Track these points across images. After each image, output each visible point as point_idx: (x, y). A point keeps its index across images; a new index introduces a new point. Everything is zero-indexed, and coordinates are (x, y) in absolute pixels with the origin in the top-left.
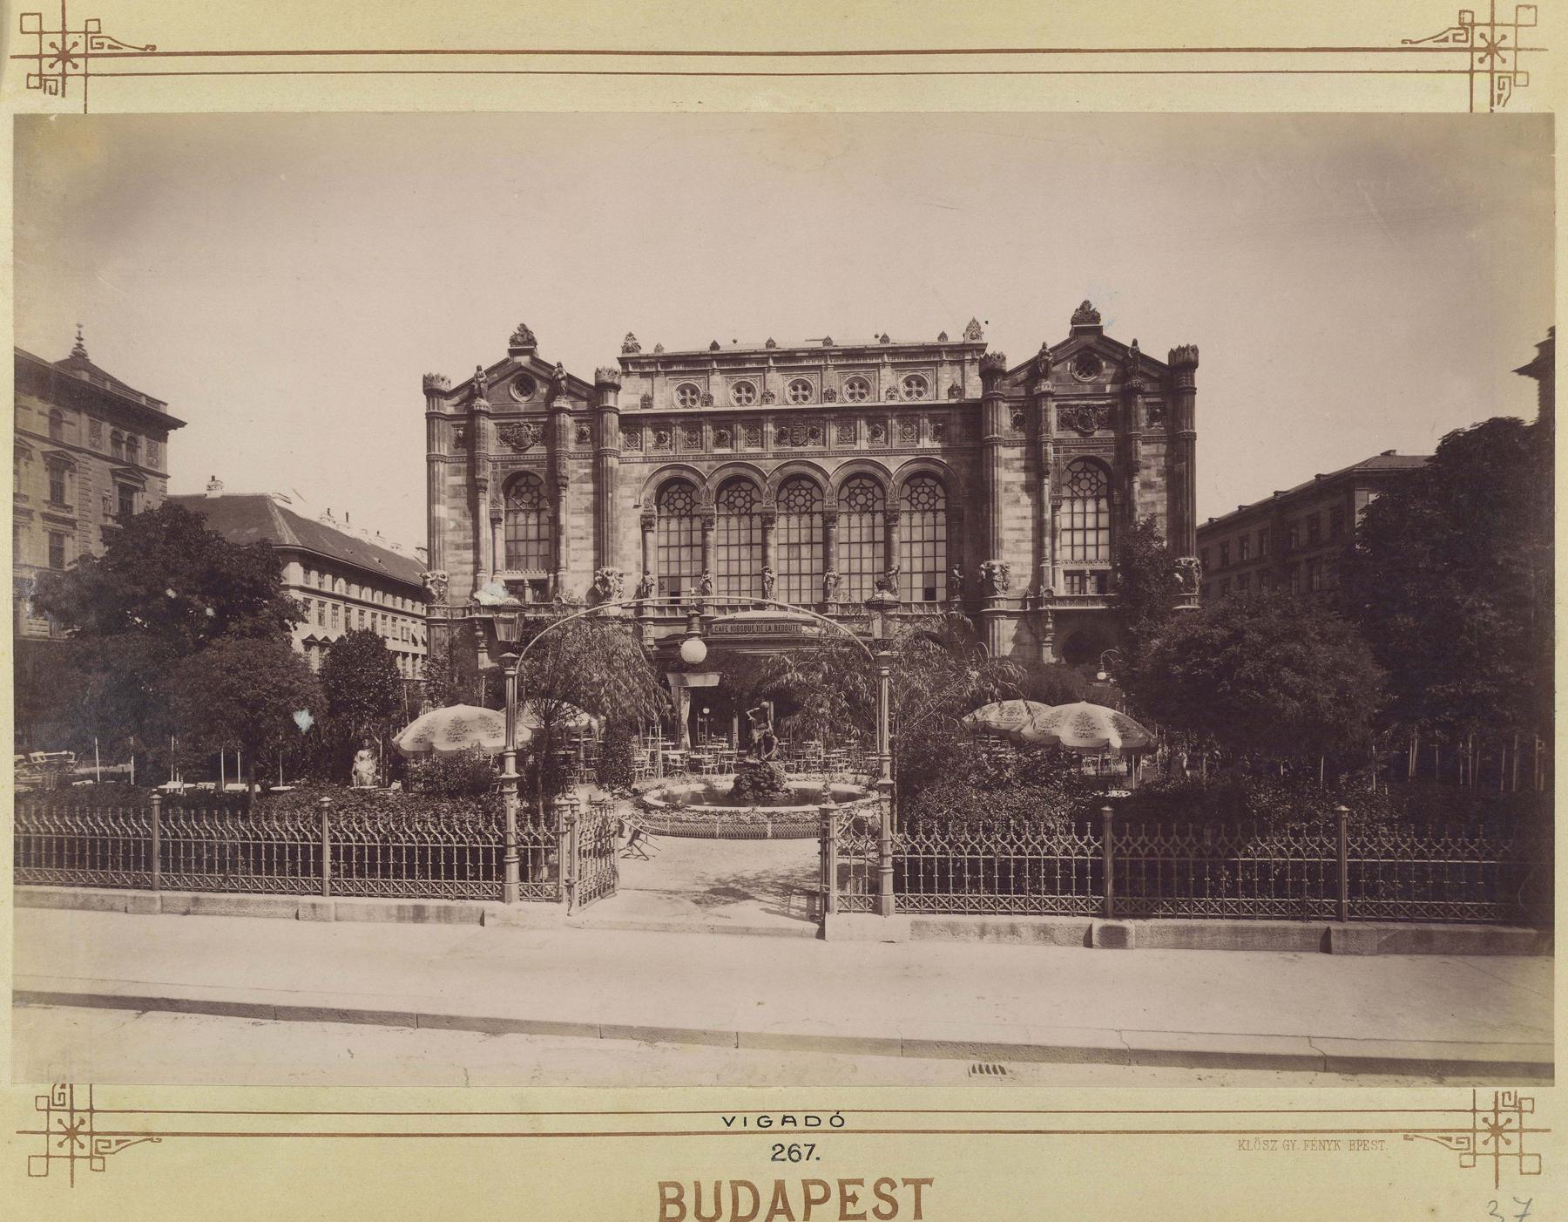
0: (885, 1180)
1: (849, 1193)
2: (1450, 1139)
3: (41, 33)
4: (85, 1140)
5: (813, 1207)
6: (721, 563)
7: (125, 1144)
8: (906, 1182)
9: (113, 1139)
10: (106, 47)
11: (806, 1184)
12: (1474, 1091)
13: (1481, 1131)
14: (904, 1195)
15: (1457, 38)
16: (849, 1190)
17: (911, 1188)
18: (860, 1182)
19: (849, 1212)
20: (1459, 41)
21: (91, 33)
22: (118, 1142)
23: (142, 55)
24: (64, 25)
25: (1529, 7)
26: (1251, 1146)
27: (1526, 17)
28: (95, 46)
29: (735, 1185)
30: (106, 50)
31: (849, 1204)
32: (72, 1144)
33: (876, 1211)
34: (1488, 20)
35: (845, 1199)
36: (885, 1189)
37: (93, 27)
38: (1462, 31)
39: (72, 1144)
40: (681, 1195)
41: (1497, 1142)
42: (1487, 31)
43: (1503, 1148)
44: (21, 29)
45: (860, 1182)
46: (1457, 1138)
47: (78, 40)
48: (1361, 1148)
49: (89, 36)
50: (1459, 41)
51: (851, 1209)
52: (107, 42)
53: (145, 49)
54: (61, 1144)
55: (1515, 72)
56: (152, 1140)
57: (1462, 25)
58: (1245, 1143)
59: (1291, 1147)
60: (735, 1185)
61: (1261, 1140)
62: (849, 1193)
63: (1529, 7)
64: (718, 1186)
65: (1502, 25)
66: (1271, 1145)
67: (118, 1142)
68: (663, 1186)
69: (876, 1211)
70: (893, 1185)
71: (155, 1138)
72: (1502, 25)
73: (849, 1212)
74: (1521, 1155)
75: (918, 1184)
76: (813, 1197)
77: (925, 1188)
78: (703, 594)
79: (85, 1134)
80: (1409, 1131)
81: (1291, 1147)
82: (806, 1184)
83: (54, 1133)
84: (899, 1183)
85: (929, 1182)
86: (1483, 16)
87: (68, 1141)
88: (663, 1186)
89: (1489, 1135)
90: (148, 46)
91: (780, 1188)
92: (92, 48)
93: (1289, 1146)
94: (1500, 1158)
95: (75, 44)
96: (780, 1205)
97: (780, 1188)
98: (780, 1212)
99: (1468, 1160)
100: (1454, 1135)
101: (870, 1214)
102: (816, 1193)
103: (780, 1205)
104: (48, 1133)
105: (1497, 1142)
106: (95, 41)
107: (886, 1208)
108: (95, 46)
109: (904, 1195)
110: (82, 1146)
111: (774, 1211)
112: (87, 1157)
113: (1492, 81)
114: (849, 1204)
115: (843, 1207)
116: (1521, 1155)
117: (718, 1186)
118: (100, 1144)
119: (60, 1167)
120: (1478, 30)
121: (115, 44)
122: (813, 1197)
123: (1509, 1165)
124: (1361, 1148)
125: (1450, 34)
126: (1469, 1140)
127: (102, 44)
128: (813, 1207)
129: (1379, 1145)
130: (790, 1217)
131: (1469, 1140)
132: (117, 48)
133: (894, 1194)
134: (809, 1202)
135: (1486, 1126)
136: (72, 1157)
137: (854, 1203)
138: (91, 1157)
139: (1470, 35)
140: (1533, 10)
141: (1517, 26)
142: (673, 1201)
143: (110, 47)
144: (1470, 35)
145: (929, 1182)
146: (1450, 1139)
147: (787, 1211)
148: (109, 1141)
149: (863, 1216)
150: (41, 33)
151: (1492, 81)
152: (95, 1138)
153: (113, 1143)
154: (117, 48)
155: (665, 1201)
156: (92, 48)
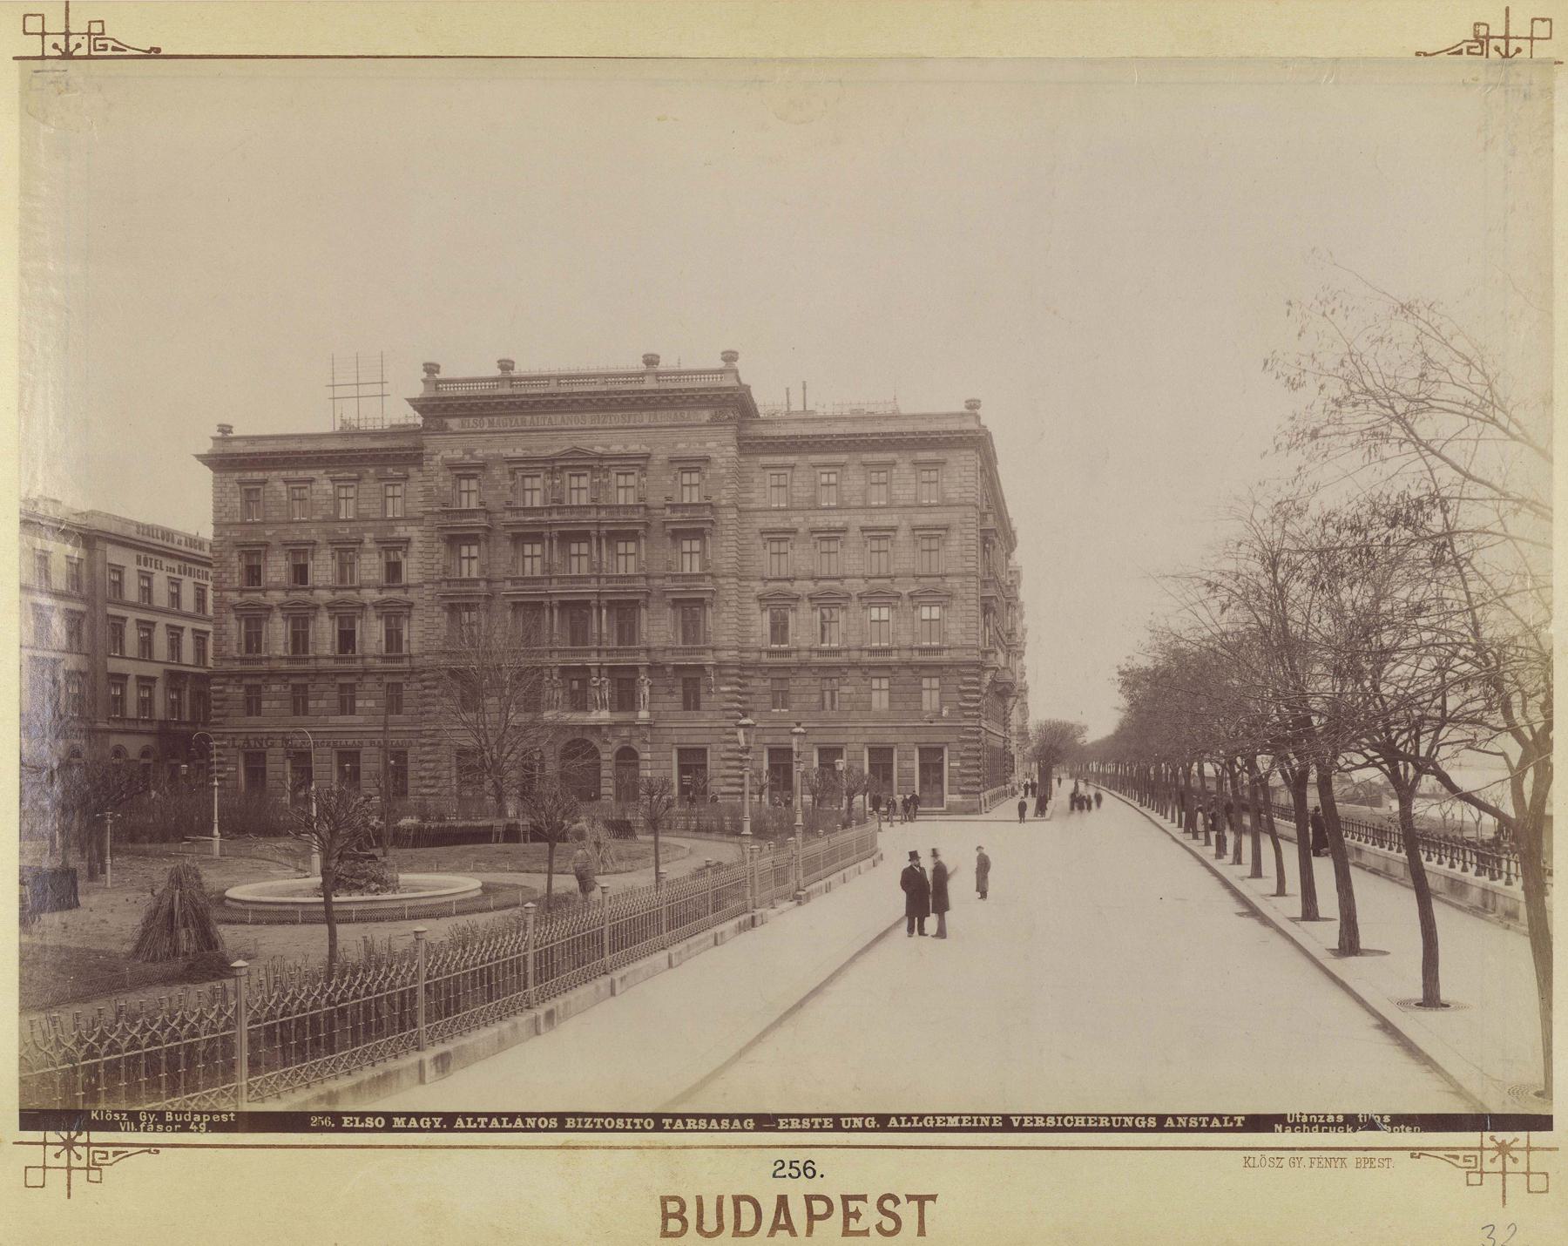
0: (891, 1197)
1: (852, 1209)
2: (1457, 1157)
3: (43, 34)
4: (82, 1151)
5: (816, 1223)
6: (685, 555)
7: (1455, 50)
8: (910, 1198)
9: (110, 1150)
10: (109, 48)
11: (809, 1199)
12: (1528, 1137)
13: (1489, 1149)
14: (908, 1212)
15: (1471, 50)
16: (853, 1206)
17: (915, 1204)
18: (863, 1198)
19: (852, 1228)
20: (102, 1152)
21: (94, 34)
22: (115, 1154)
23: (1423, 1149)
24: (67, 27)
25: (1543, 20)
26: (1257, 1163)
27: (1541, 29)
28: (1473, 1159)
29: (737, 1200)
30: (109, 52)
31: (852, 1220)
32: (69, 1155)
33: (879, 1227)
34: (74, 1173)
35: (847, 1215)
36: (889, 1205)
37: (96, 28)
38: (1477, 44)
39: (69, 1155)
40: (683, 1208)
41: (67, 46)
42: (75, 1163)
43: (1510, 1166)
44: (24, 30)
45: (863, 1198)
46: (106, 50)
47: (81, 41)
48: (1369, 1165)
49: (93, 37)
50: (102, 1152)
51: (854, 1225)
52: (1460, 1162)
53: (149, 51)
54: (57, 1155)
55: (1482, 1172)
56: (149, 1151)
57: (1477, 38)
58: (1251, 1161)
59: (1297, 1165)
60: (737, 1200)
61: (1267, 1158)
62: (852, 1209)
63: (1543, 20)
64: (720, 1200)
65: (1517, 38)
66: (1276, 1162)
67: (115, 1154)
68: (664, 1201)
69: (879, 1227)
70: (897, 1201)
71: (152, 1149)
72: (1517, 38)
73: (852, 1228)
74: (1528, 1173)
75: (921, 1200)
76: (816, 1212)
77: (928, 1203)
78: (250, 606)
79: (82, 1145)
80: (1418, 1149)
81: (1297, 1165)
82: (809, 1199)
83: (51, 1144)
84: (903, 1199)
85: (933, 1198)
86: (79, 1177)
87: (65, 1152)
88: (664, 1201)
89: (1496, 1153)
90: (152, 49)
91: (782, 1201)
92: (1476, 1157)
93: (1294, 1162)
94: (1507, 1176)
95: (78, 46)
96: (782, 1221)
97: (782, 1201)
98: (783, 1228)
99: (1475, 1178)
100: (1461, 1154)
101: (873, 1231)
102: (819, 1207)
103: (782, 1221)
104: (1504, 1173)
105: (67, 46)
106: (98, 42)
107: (889, 1205)
108: (98, 47)
109: (908, 1212)
110: (79, 1157)
111: (776, 1227)
112: (1493, 37)
113: (1470, 1149)
114: (852, 1220)
115: (846, 1224)
116: (1528, 1173)
117: (720, 1200)
118: (97, 1155)
119: (1519, 27)
120: (1493, 43)
121: (1451, 1159)
122: (816, 1212)
123: (1515, 1183)
124: (1369, 1165)
125: (111, 1159)
126: (1476, 1159)
127: (1465, 1161)
128: (816, 1223)
129: (1386, 1163)
130: (793, 1233)
131: (1476, 1159)
132: (1449, 1156)
133: (897, 1210)
134: (811, 1217)
135: (1514, 1154)
136: (69, 1168)
137: (857, 1219)
138: (88, 1168)
139: (91, 1159)
140: (962, 466)
141: (1532, 39)
142: (674, 1216)
143: (114, 49)
144: (91, 1159)
145: (933, 1198)
146: (114, 49)
147: (789, 1226)
148: (106, 1153)
149: (866, 1233)
150: (43, 34)
151: (1470, 1149)
152: (92, 1149)
153: (110, 1154)
154: (1449, 1156)
155: (666, 1216)
156: (95, 50)
